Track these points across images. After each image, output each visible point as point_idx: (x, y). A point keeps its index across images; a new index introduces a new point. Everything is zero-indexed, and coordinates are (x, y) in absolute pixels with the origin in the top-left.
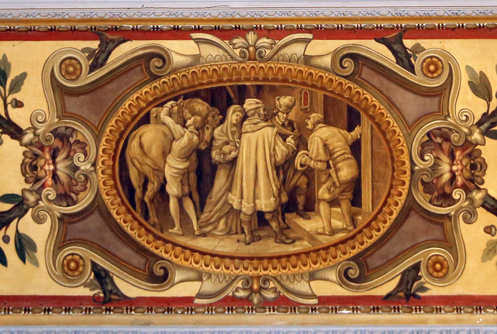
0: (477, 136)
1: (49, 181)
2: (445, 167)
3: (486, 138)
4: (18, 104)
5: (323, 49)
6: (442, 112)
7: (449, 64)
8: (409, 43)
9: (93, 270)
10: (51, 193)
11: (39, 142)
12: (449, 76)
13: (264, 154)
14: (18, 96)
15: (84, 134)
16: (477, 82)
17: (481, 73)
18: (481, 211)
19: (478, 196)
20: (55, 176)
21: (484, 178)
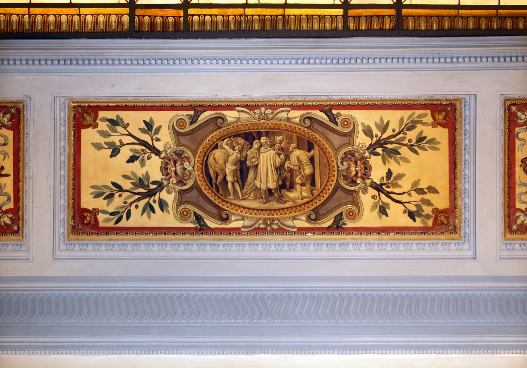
0: (367, 154)
1: (173, 175)
4: (158, 140)
11: (168, 157)
14: (158, 136)
15: (188, 153)
16: (366, 129)
17: (368, 125)
18: (370, 189)
19: (368, 182)
20: (176, 172)
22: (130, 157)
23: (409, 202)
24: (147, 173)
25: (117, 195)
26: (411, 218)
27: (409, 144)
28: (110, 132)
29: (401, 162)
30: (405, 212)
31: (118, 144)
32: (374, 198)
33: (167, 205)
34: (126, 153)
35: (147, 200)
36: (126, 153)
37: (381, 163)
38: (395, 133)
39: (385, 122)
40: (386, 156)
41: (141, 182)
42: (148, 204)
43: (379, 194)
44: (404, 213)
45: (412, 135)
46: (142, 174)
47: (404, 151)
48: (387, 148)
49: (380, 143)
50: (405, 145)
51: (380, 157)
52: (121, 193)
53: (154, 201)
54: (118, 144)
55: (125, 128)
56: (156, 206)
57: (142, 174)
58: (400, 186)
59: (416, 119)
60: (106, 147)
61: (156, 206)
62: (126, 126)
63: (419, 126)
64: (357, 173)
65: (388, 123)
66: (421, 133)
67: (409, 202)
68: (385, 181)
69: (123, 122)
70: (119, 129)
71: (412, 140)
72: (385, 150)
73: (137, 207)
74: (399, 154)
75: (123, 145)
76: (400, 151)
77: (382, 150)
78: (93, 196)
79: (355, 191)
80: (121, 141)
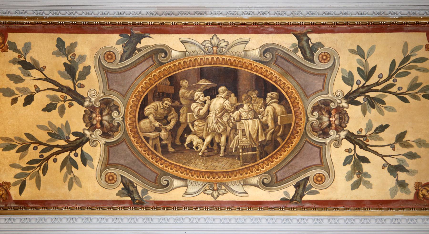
1: (98, 125)
3: (349, 105)
4: (349, 151)
7: (334, 57)
8: (314, 38)
10: (98, 132)
11: (93, 105)
12: (333, 65)
13: (210, 16)
14: (348, 154)
15: (117, 100)
16: (347, 76)
17: (350, 71)
18: (345, 142)
19: (343, 134)
20: (101, 122)
21: (347, 124)
23: (390, 156)
27: (399, 92)
28: (22, 76)
29: (47, 125)
31: (33, 90)
33: (344, 78)
34: (41, 99)
36: (41, 99)
37: (360, 113)
39: (371, 67)
40: (368, 106)
41: (373, 103)
42: (367, 80)
44: (383, 168)
45: (403, 83)
48: (369, 96)
49: (72, 147)
50: (41, 144)
51: (359, 107)
52: (36, 145)
54: (397, 146)
55: (387, 163)
56: (357, 77)
59: (412, 64)
60: (410, 142)
61: (78, 160)
62: (41, 70)
63: (24, 165)
64: (101, 113)
65: (374, 68)
66: (21, 158)
67: (390, 156)
69: (389, 170)
70: (34, 73)
71: (402, 88)
75: (38, 90)
76: (384, 99)
77: (69, 138)
79: (325, 143)
80: (36, 87)
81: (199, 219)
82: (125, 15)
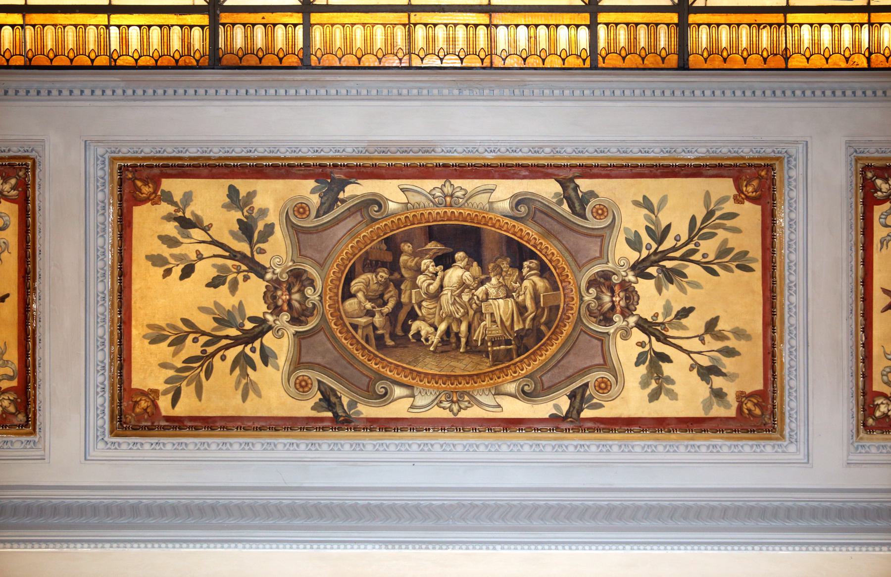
0: (270, 318)
2: (606, 298)
4: (641, 344)
5: (399, 408)
6: (603, 256)
8: (585, 185)
9: (319, 389)
10: (285, 317)
11: (277, 278)
14: (641, 350)
15: (313, 272)
18: (635, 330)
19: (632, 320)
22: (214, 278)
23: (699, 353)
24: (241, 303)
25: (711, 257)
26: (638, 358)
28: (179, 237)
30: (691, 368)
31: (193, 256)
32: (261, 249)
34: (205, 270)
35: (240, 348)
36: (205, 270)
37: (654, 291)
38: (679, 244)
41: (671, 276)
42: (660, 243)
43: (650, 341)
45: (708, 248)
46: (667, 289)
47: (693, 271)
49: (247, 338)
50: (204, 334)
53: (648, 247)
54: (708, 338)
56: (646, 239)
57: (667, 289)
58: (214, 266)
60: (725, 333)
61: (256, 357)
63: (180, 365)
65: (669, 227)
66: (175, 354)
67: (699, 353)
68: (240, 277)
69: (699, 374)
72: (240, 327)
73: (223, 358)
74: (684, 276)
75: (200, 257)
76: (686, 271)
78: (750, 255)
80: (198, 253)
81: (432, 445)
82: (322, 153)
